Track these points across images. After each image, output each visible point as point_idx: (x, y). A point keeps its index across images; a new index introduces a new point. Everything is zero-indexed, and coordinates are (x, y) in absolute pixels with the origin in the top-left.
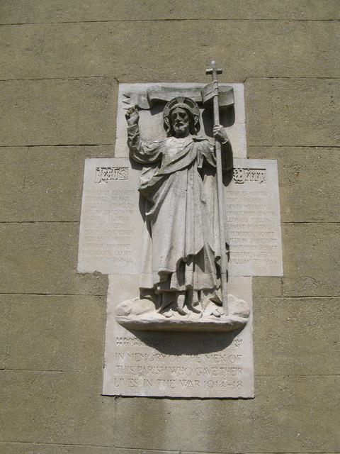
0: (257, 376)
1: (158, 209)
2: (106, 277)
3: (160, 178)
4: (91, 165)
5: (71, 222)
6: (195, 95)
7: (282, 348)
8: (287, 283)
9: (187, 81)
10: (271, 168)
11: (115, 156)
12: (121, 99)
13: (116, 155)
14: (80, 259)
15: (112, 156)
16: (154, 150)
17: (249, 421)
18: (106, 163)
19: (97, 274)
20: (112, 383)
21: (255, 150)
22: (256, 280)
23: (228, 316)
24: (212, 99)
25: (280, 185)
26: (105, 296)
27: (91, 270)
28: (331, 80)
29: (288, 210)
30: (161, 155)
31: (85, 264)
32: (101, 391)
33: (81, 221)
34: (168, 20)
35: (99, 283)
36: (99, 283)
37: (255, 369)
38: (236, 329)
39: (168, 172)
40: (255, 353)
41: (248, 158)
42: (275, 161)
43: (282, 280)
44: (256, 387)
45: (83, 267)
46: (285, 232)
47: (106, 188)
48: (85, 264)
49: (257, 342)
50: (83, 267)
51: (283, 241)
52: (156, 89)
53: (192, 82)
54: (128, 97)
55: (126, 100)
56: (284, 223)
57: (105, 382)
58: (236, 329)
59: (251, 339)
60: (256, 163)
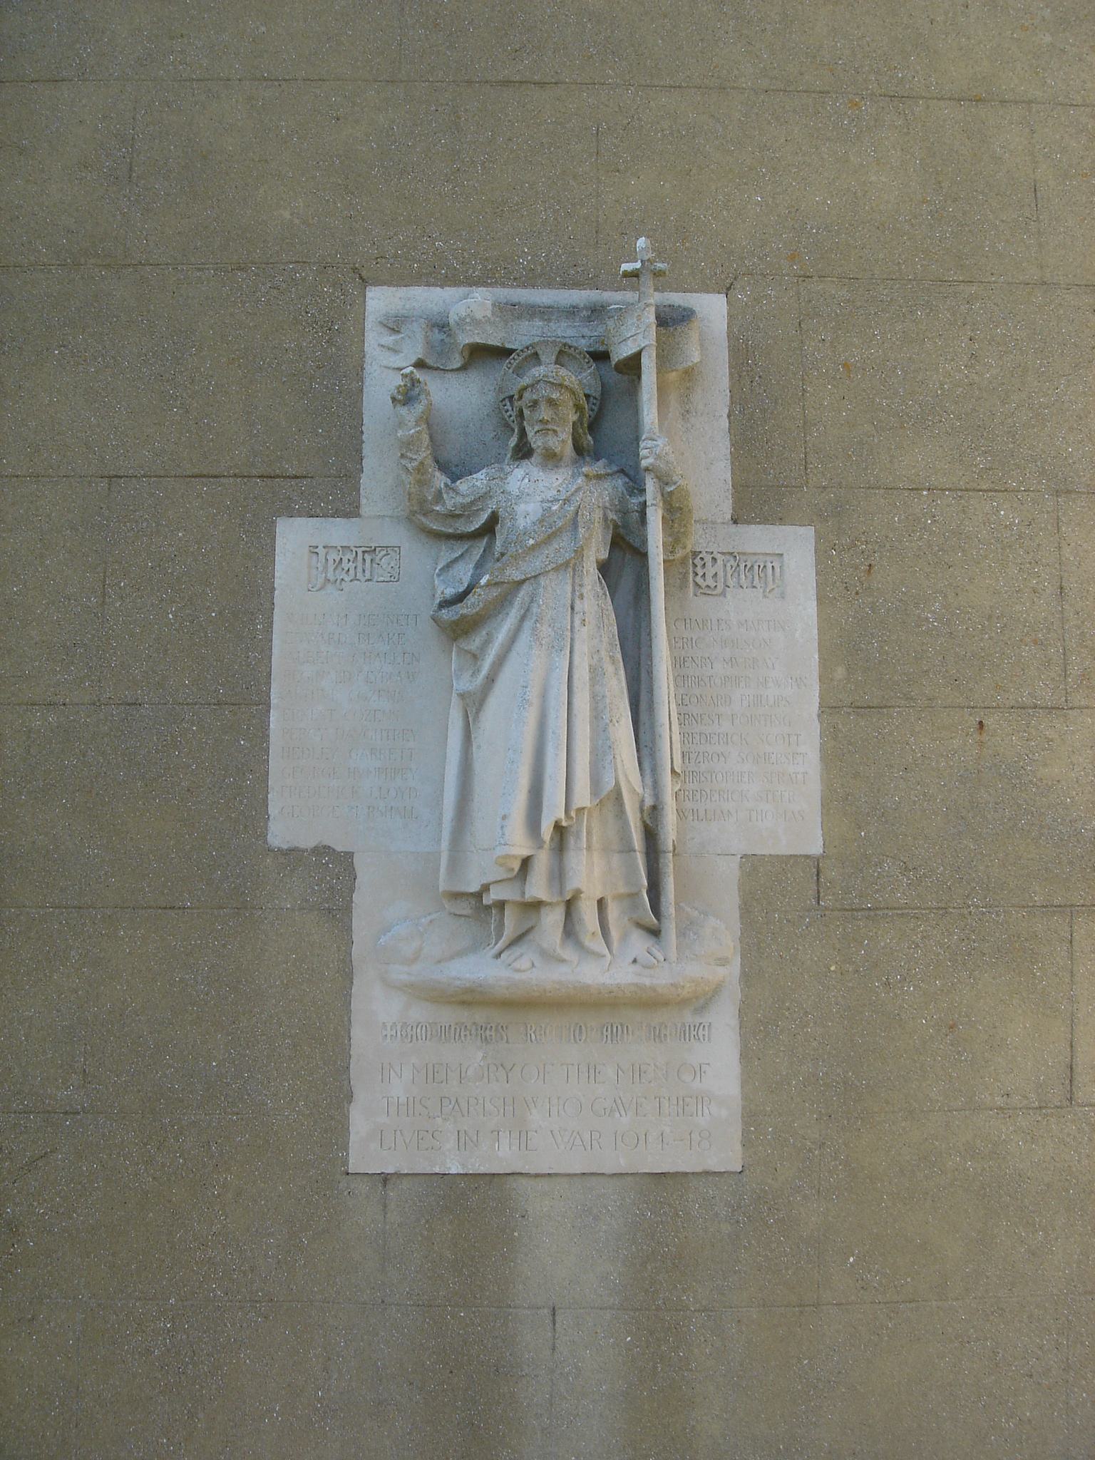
0: (751, 1117)
1: (491, 680)
2: (345, 862)
3: (495, 592)
4: (296, 541)
5: (241, 697)
6: (586, 331)
7: (815, 1044)
8: (831, 873)
9: (565, 284)
10: (794, 549)
11: (363, 511)
12: (374, 339)
13: (364, 510)
14: (273, 810)
15: (350, 510)
16: (472, 503)
17: (726, 1228)
18: (338, 532)
19: (323, 851)
20: (379, 1135)
21: (756, 501)
22: (752, 865)
23: (670, 969)
24: (637, 356)
25: (821, 600)
26: (348, 909)
27: (307, 842)
28: (973, 289)
29: (840, 672)
30: (494, 519)
31: (287, 826)
32: (346, 1163)
33: (274, 700)
34: (506, 83)
35: (331, 874)
36: (331, 874)
37: (745, 1097)
38: (701, 1000)
39: (518, 576)
40: (745, 1056)
41: (735, 522)
42: (808, 532)
43: (816, 865)
44: (746, 1143)
45: (281, 833)
46: (831, 733)
47: (327, 594)
48: (287, 826)
49: (757, 1035)
50: (281, 833)
51: (823, 758)
52: (472, 307)
53: (577, 285)
54: (394, 331)
55: (389, 339)
56: (828, 709)
57: (353, 1138)
58: (701, 1000)
59: (734, 1022)
60: (757, 538)
